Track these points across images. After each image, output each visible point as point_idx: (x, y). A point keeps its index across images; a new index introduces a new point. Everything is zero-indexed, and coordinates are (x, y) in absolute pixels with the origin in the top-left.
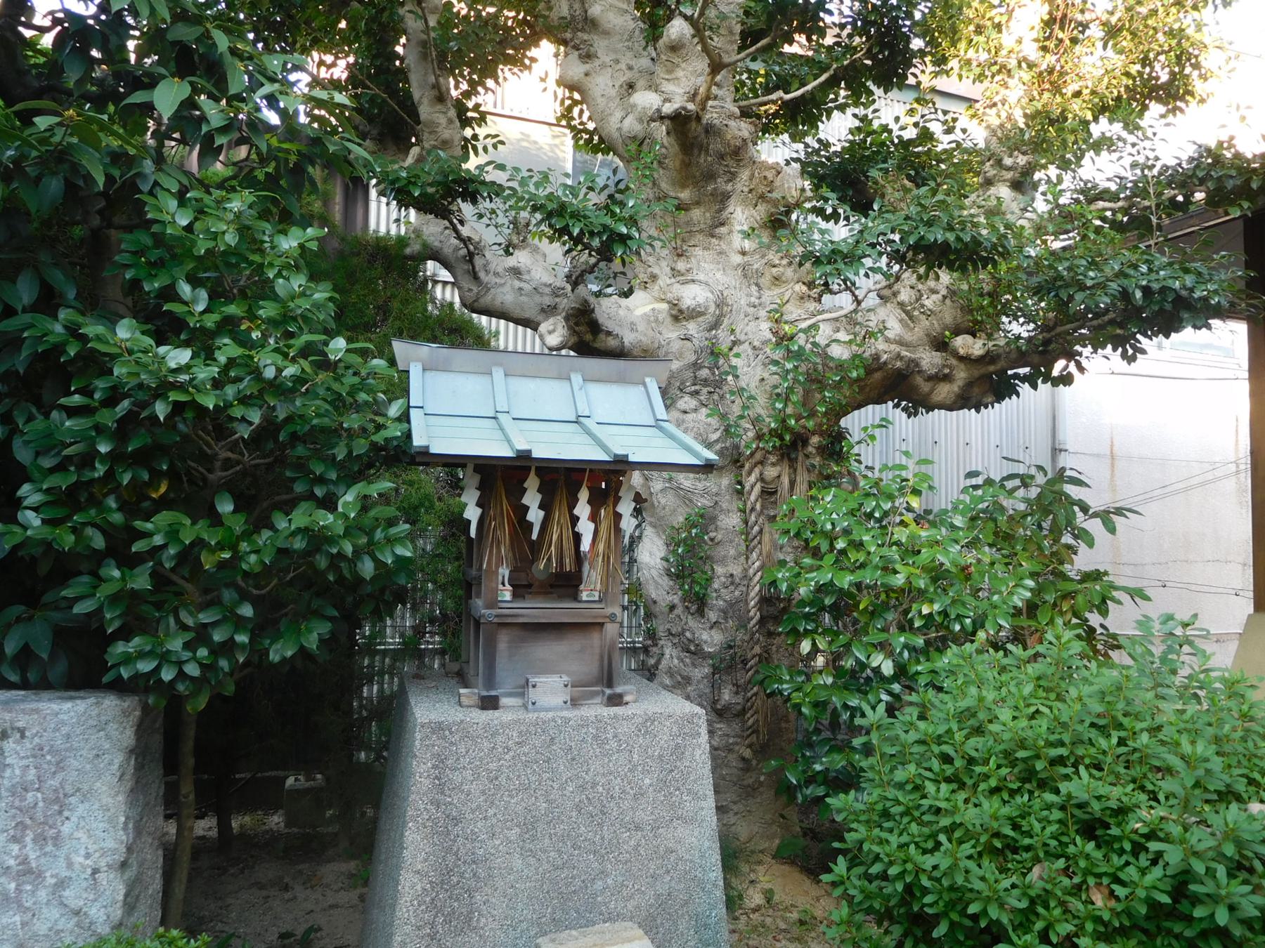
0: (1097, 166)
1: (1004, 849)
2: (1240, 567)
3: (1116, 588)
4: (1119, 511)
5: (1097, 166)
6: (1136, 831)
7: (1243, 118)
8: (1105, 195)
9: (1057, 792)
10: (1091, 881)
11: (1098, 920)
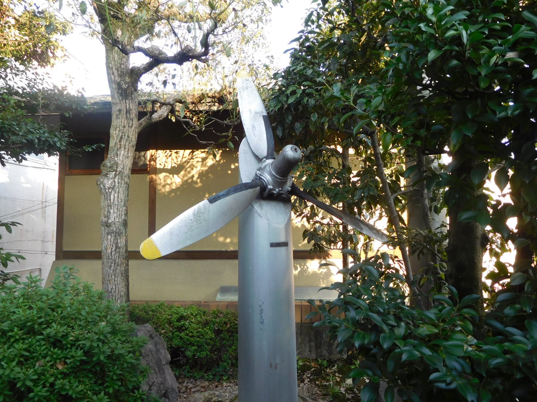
0: (15, 81)
1: (24, 361)
2: (41, 242)
3: (12, 255)
4: (13, 224)
5: (15, 81)
6: (72, 340)
7: (71, 81)
8: (17, 93)
9: (42, 334)
10: (58, 361)
11: (62, 373)
